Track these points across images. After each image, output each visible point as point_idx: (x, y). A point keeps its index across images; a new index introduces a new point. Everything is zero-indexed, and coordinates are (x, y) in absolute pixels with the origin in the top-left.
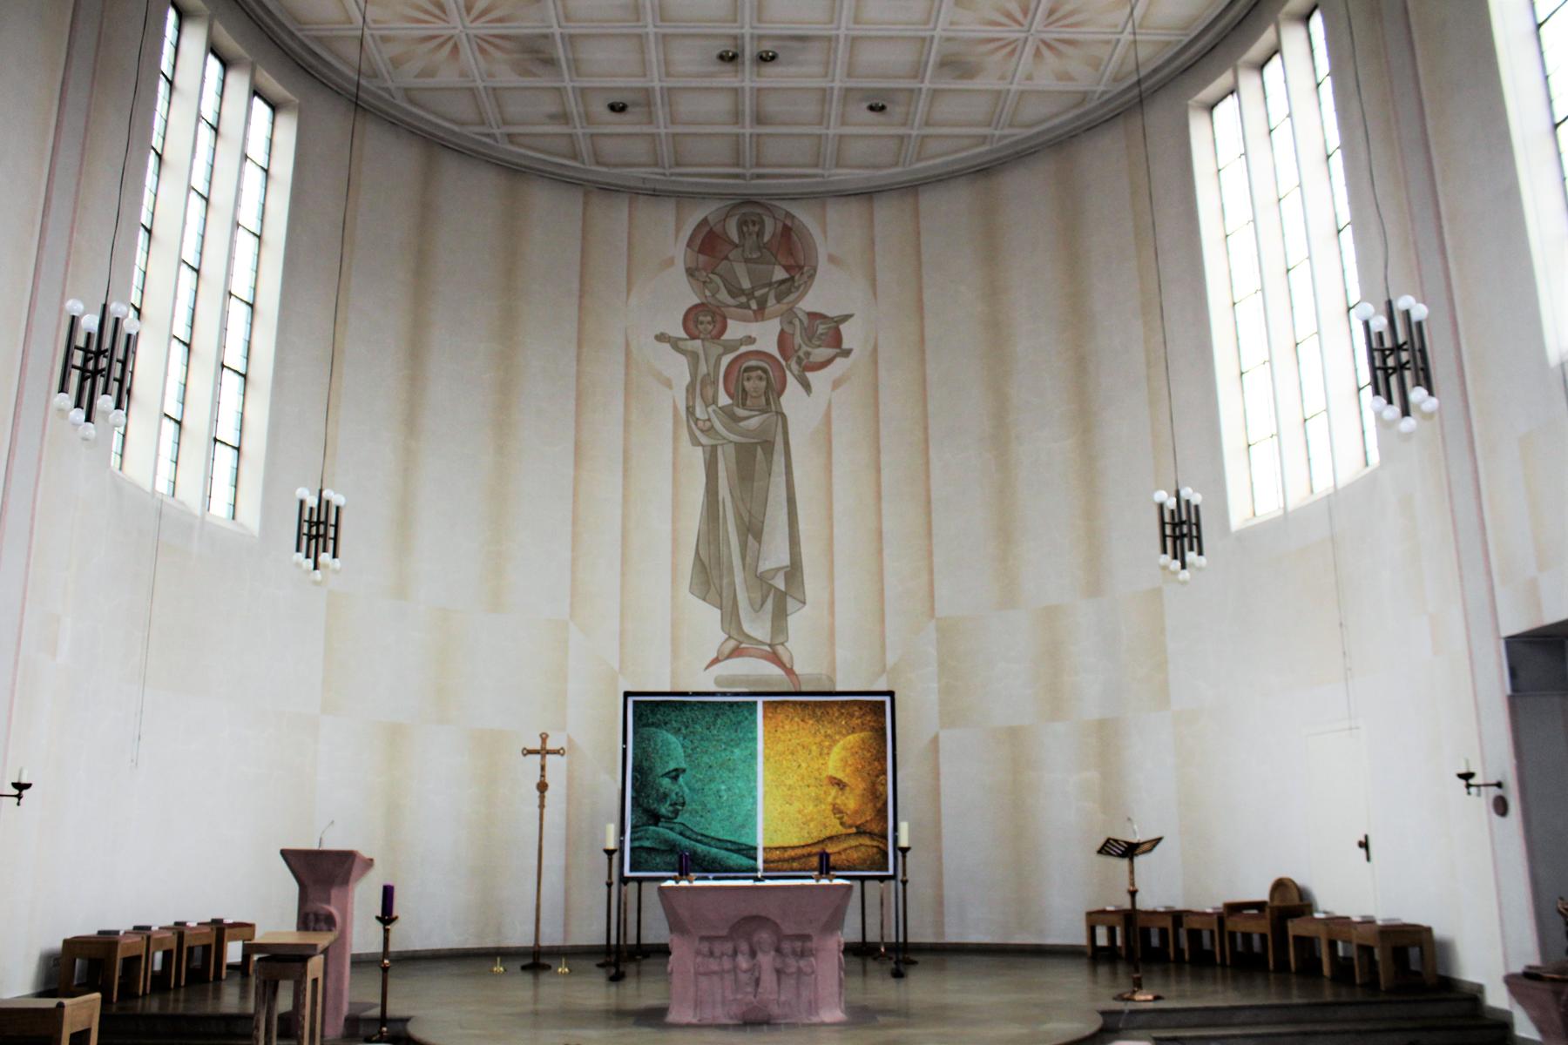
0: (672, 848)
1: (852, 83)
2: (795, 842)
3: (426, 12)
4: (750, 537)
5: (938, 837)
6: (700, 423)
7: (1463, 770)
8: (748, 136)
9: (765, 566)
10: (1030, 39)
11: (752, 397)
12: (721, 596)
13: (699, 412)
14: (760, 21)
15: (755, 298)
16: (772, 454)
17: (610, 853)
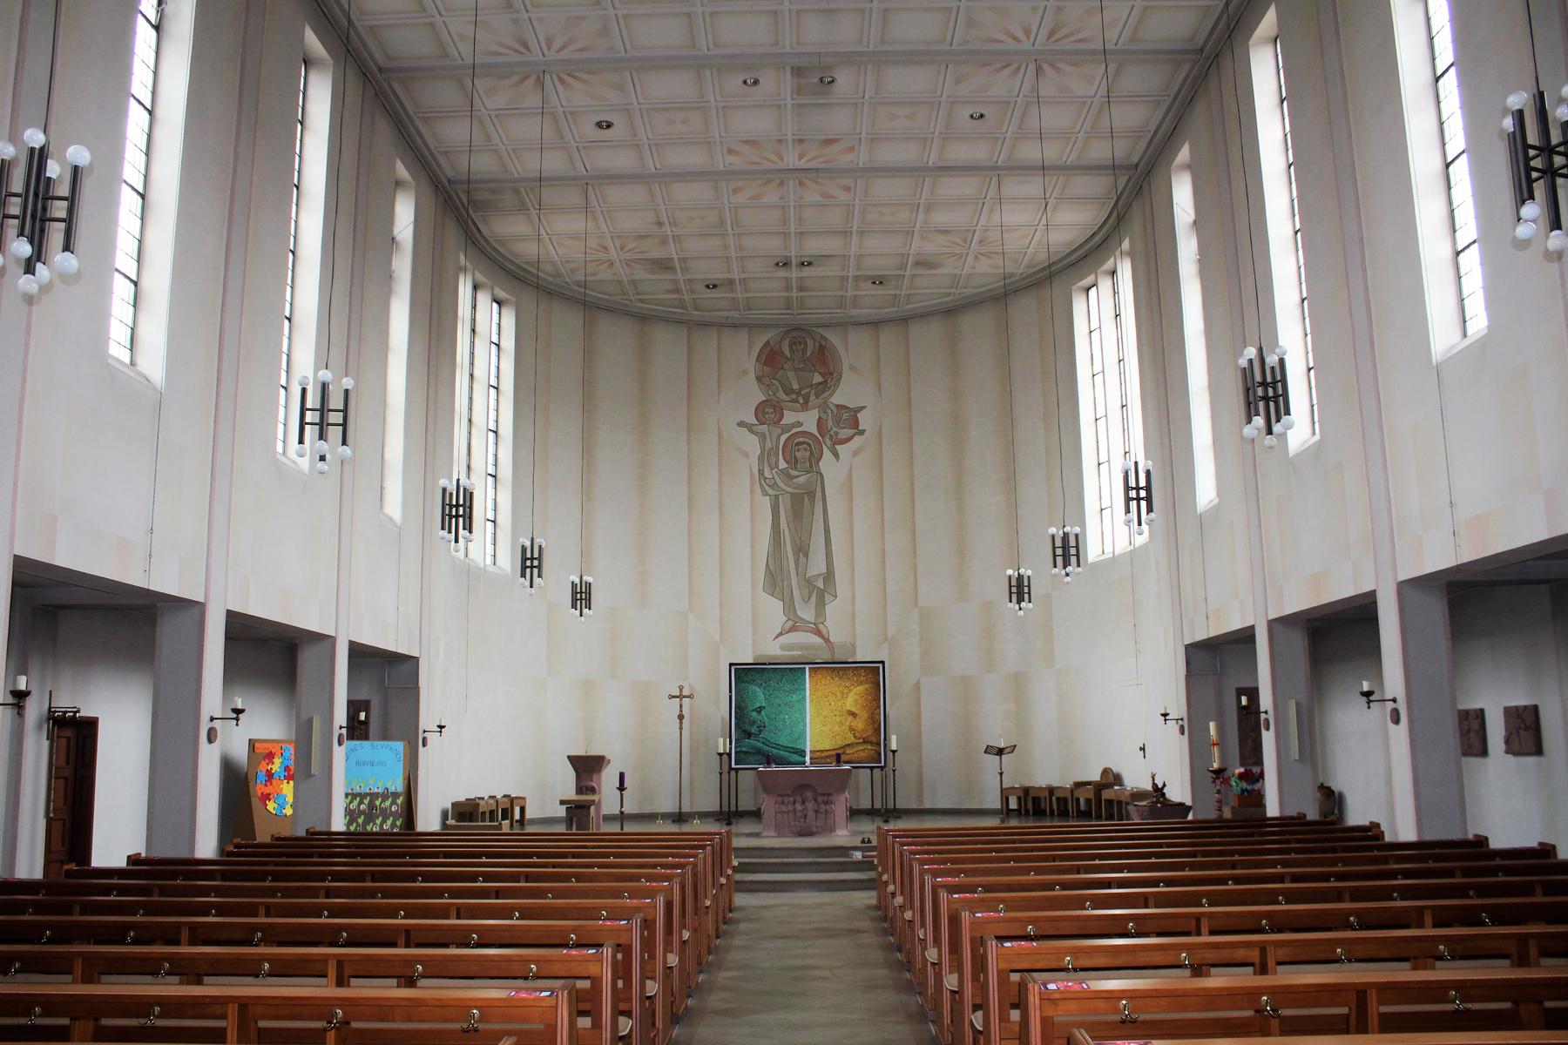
0: (759, 752)
1: (859, 273)
2: (828, 748)
3: (596, 250)
4: (801, 555)
5: (919, 745)
6: (768, 481)
7: (1163, 712)
8: (793, 102)
9: (811, 572)
10: (970, 254)
11: (801, 462)
12: (783, 593)
13: (767, 474)
14: (800, 225)
15: (801, 395)
16: (814, 502)
17: (721, 755)
